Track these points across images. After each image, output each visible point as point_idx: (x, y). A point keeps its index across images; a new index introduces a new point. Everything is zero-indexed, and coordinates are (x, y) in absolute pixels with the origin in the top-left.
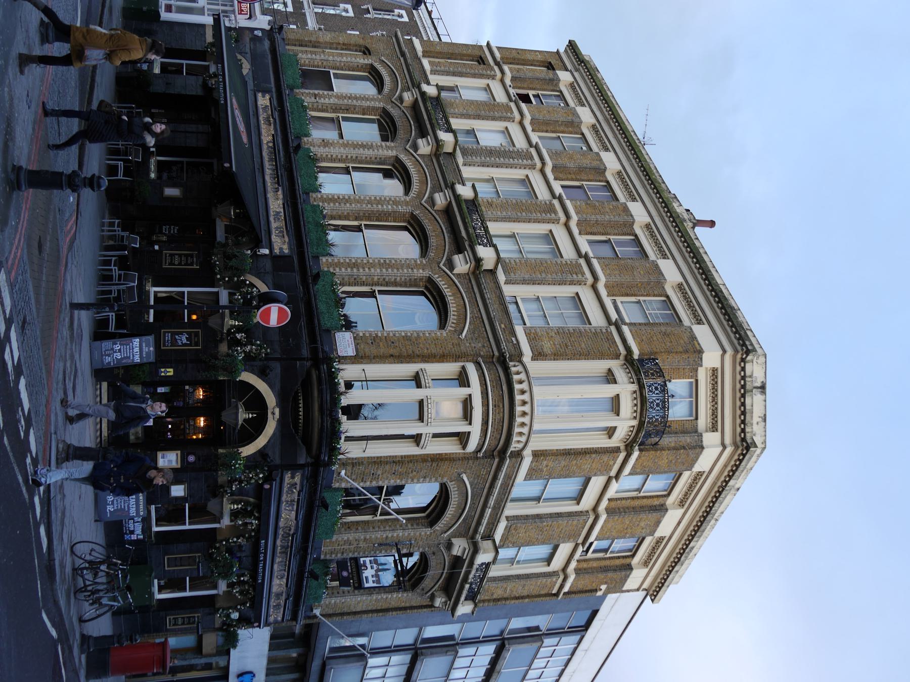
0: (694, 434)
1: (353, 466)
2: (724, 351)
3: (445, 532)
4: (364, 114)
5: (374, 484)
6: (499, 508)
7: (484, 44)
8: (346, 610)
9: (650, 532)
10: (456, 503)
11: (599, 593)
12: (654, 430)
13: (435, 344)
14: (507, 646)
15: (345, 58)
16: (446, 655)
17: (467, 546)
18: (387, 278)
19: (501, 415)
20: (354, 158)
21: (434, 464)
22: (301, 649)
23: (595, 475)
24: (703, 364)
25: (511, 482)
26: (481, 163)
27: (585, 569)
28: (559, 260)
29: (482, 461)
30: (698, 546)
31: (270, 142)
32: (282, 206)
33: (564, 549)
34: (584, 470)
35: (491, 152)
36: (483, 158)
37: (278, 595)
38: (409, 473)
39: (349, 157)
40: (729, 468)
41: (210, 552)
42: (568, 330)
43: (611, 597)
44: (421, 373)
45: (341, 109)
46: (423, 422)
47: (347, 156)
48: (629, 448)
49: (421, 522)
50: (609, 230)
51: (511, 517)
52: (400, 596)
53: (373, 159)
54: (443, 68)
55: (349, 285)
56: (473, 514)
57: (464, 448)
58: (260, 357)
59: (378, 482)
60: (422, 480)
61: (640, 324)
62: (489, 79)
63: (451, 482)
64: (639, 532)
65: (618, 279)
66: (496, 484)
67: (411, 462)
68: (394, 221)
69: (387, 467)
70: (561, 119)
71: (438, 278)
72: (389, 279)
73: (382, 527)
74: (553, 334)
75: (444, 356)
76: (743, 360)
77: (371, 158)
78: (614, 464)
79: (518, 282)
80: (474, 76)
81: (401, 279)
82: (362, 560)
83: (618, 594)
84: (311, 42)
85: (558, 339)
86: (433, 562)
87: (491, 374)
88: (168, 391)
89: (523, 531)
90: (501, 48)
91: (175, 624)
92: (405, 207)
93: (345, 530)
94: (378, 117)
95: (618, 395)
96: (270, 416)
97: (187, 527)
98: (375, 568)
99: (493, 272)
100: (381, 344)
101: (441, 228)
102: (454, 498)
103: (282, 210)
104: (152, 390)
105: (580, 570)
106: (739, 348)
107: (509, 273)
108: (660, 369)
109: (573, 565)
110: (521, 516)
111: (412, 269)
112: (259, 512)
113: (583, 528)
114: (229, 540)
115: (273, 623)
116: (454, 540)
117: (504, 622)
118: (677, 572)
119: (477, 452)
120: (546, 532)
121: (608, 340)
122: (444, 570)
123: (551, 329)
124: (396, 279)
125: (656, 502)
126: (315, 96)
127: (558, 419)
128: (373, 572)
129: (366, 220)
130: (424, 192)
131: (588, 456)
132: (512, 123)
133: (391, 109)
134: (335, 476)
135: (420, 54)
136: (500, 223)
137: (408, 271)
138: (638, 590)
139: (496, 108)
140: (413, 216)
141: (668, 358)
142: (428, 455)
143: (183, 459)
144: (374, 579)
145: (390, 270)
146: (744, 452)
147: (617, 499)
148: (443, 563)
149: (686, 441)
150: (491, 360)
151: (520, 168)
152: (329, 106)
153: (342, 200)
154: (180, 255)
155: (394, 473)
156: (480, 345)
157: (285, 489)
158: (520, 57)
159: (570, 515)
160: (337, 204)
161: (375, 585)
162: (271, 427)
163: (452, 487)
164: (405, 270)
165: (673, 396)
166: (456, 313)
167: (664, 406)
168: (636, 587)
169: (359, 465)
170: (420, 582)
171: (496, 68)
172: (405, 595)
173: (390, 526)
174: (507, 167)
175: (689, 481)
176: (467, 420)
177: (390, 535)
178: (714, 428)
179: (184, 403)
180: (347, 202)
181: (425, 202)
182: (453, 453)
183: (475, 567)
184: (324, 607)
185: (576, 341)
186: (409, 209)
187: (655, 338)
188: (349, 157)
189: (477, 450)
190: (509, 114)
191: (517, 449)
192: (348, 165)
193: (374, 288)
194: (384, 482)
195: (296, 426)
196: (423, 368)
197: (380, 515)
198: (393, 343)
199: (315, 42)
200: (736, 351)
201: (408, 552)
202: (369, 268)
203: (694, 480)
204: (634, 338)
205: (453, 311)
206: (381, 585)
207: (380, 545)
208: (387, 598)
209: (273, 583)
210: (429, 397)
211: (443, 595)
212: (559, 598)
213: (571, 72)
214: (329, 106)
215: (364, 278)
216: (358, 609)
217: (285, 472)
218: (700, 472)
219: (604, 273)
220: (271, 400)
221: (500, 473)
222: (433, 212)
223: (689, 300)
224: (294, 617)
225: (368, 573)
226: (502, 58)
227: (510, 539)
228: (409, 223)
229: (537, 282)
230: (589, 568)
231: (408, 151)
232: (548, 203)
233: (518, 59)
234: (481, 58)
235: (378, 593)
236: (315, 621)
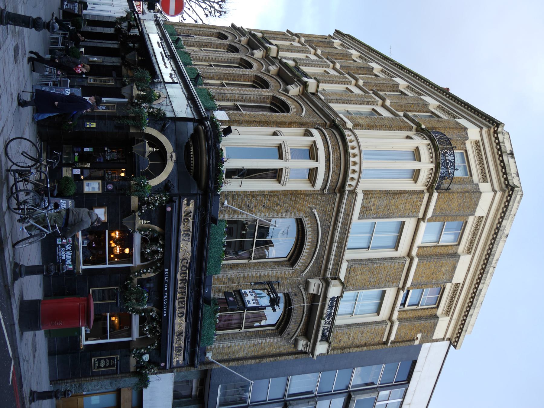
3: (304, 272)
6: (342, 247)
7: (285, 31)
8: (231, 356)
11: (417, 343)
14: (353, 396)
16: (308, 405)
17: (320, 283)
18: (244, 96)
20: (214, 59)
22: (197, 405)
25: (349, 220)
37: (180, 334)
38: (275, 207)
39: (211, 58)
40: (501, 211)
41: (126, 283)
47: (209, 58)
48: (430, 189)
56: (323, 253)
57: (313, 186)
58: (160, 115)
60: (284, 214)
63: (306, 217)
66: (339, 217)
68: (245, 81)
72: (246, 97)
78: (421, 205)
79: (333, 101)
81: (254, 97)
83: (430, 344)
88: (91, 151)
91: (99, 367)
95: (417, 148)
96: (168, 158)
97: (109, 341)
104: (80, 149)
106: (491, 125)
112: (163, 240)
113: (402, 272)
114: (140, 271)
118: (471, 315)
120: (376, 275)
122: (304, 303)
125: (451, 251)
128: (253, 298)
138: (443, 339)
142: (288, 191)
143: (104, 187)
146: (511, 193)
147: (424, 247)
152: (195, 43)
154: (105, 359)
157: (183, 217)
161: (255, 305)
162: (170, 167)
168: (442, 337)
169: (238, 197)
172: (276, 340)
175: (473, 229)
178: (485, 180)
179: (104, 159)
182: (306, 191)
184: (215, 352)
188: (211, 58)
195: (189, 169)
200: (489, 128)
203: (476, 227)
206: (260, 305)
208: (262, 343)
209: (176, 322)
210: (285, 142)
211: (304, 339)
214: (195, 43)
215: (229, 96)
220: (169, 148)
221: (342, 205)
227: (351, 281)
228: (254, 82)
229: (345, 102)
236: (208, 367)
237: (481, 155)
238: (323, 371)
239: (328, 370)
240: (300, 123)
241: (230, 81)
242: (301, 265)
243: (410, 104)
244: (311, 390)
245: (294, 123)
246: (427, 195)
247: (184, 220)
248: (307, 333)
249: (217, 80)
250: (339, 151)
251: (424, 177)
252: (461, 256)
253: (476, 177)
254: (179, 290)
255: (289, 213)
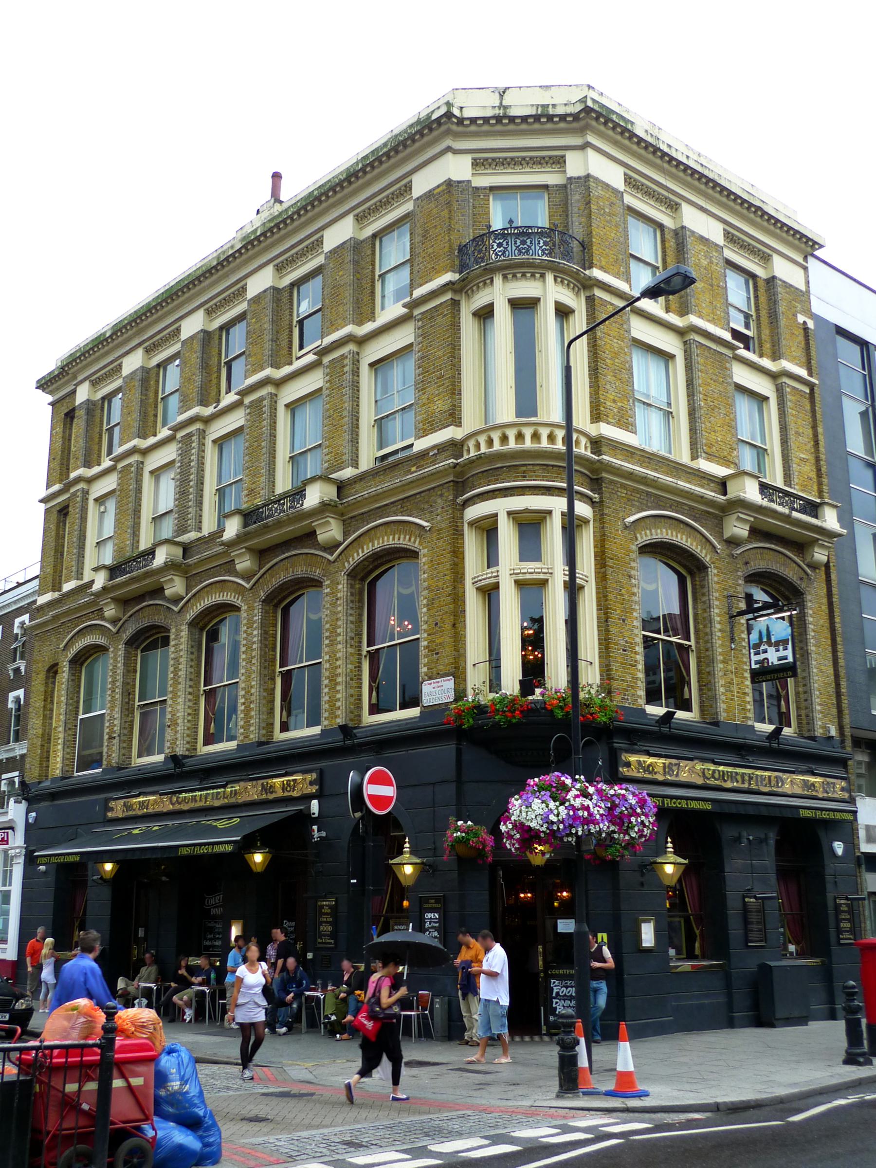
0: (569, 190)
1: (612, 678)
2: (449, 149)
3: (714, 547)
4: (135, 671)
5: (640, 649)
8: (832, 689)
9: (717, 251)
10: (669, 532)
11: (811, 324)
12: (560, 248)
13: (438, 564)
15: (62, 698)
17: (735, 516)
19: (538, 468)
20: (191, 683)
21: (610, 563)
23: (628, 331)
24: (467, 179)
26: (196, 506)
27: (774, 346)
28: (325, 392)
29: (606, 495)
30: (739, 183)
31: (171, 799)
32: (254, 782)
33: (742, 376)
34: (621, 348)
35: (182, 494)
36: (190, 503)
38: (624, 600)
39: (190, 690)
42: (419, 375)
43: (817, 307)
44: (479, 584)
45: (128, 703)
46: (547, 580)
47: (190, 693)
49: (700, 581)
50: (285, 323)
51: (692, 453)
52: (810, 612)
53: (193, 657)
54: (73, 563)
55: (360, 687)
56: (686, 508)
59: (636, 644)
60: (633, 581)
61: (411, 273)
62: (87, 499)
63: (637, 539)
64: (718, 267)
65: (349, 307)
67: (607, 596)
69: (613, 630)
70: (138, 396)
71: (349, 562)
72: (352, 631)
73: (706, 638)
74: (425, 396)
75: (454, 552)
76: (461, 121)
77: (192, 660)
78: (612, 304)
79: (354, 449)
80: (84, 519)
81: (351, 615)
82: (754, 666)
83: (812, 297)
84: (42, 746)
85: (432, 390)
86: (760, 564)
87: (480, 484)
89: (713, 436)
90: (47, 484)
92: (256, 611)
93: (709, 690)
94: (139, 652)
98: (766, 647)
99: (341, 487)
100: (438, 641)
101: (282, 560)
102: (662, 534)
103: (260, 782)
105: (774, 353)
107: (342, 462)
108: (474, 240)
109: (766, 363)
110: (691, 438)
111: (337, 599)
115: (850, 793)
116: (727, 535)
117: (852, 461)
119: (593, 502)
121: (433, 317)
123: (418, 399)
124: (352, 622)
125: (671, 244)
126: (111, 738)
127: (544, 386)
128: (771, 650)
129: (275, 666)
130: (235, 585)
131: (599, 342)
132: (145, 464)
133: (128, 634)
134: (627, 705)
135: (56, 595)
136: (276, 477)
137: (340, 605)
138: (805, 269)
139: (125, 487)
140: (266, 601)
141: (459, 231)
142: (597, 573)
144: (781, 648)
145: (339, 631)
146: (594, 115)
148: (761, 550)
149: (578, 201)
150: (461, 485)
151: (204, 451)
153: (246, 699)
155: (624, 620)
156: (439, 501)
158: (59, 457)
159: (689, 367)
160: (252, 706)
161: (790, 646)
163: (645, 537)
164: (339, 609)
165: (511, 222)
166: (397, 536)
167: (525, 234)
168: (801, 272)
170: (791, 583)
171: (72, 490)
172: (809, 604)
173: (705, 626)
174: (203, 470)
176: (545, 518)
177: (718, 626)
178: (560, 161)
180: (249, 691)
181: (248, 583)
183: (765, 503)
185: (434, 364)
186: (258, 605)
187: (430, 250)
188: (190, 690)
189: (590, 502)
190: (133, 469)
191: (588, 445)
192: (202, 692)
193: (364, 653)
194: (636, 635)
196: (471, 581)
197: (689, 641)
198: (436, 624)
199: (43, 740)
200: (448, 132)
201: (744, 601)
202: (337, 660)
203: (638, 189)
204: (431, 280)
205: (394, 539)
206: (790, 638)
207: (732, 640)
208: (814, 631)
212: (817, 382)
213: (77, 385)
215: (349, 666)
216: (831, 671)
217: (620, 776)
218: (625, 181)
219: (342, 328)
222: (262, 571)
223: (378, 204)
224: (842, 763)
225: (773, 656)
226: (60, 481)
229: (355, 422)
230: (772, 340)
231: (182, 608)
232: (248, 411)
233: (62, 458)
234: (60, 511)
235: (807, 643)
237: (505, 159)
238: (852, 515)
239: (851, 505)
240: (454, 534)
241: (275, 655)
242: (704, 551)
243: (356, 281)
244: (871, 537)
245: (455, 547)
246: (598, 293)
247: (650, 773)
248: (801, 546)
249: (275, 684)
250: (531, 467)
251: (568, 297)
252: (684, 224)
253: (553, 179)
254: (746, 785)
255: (633, 572)
